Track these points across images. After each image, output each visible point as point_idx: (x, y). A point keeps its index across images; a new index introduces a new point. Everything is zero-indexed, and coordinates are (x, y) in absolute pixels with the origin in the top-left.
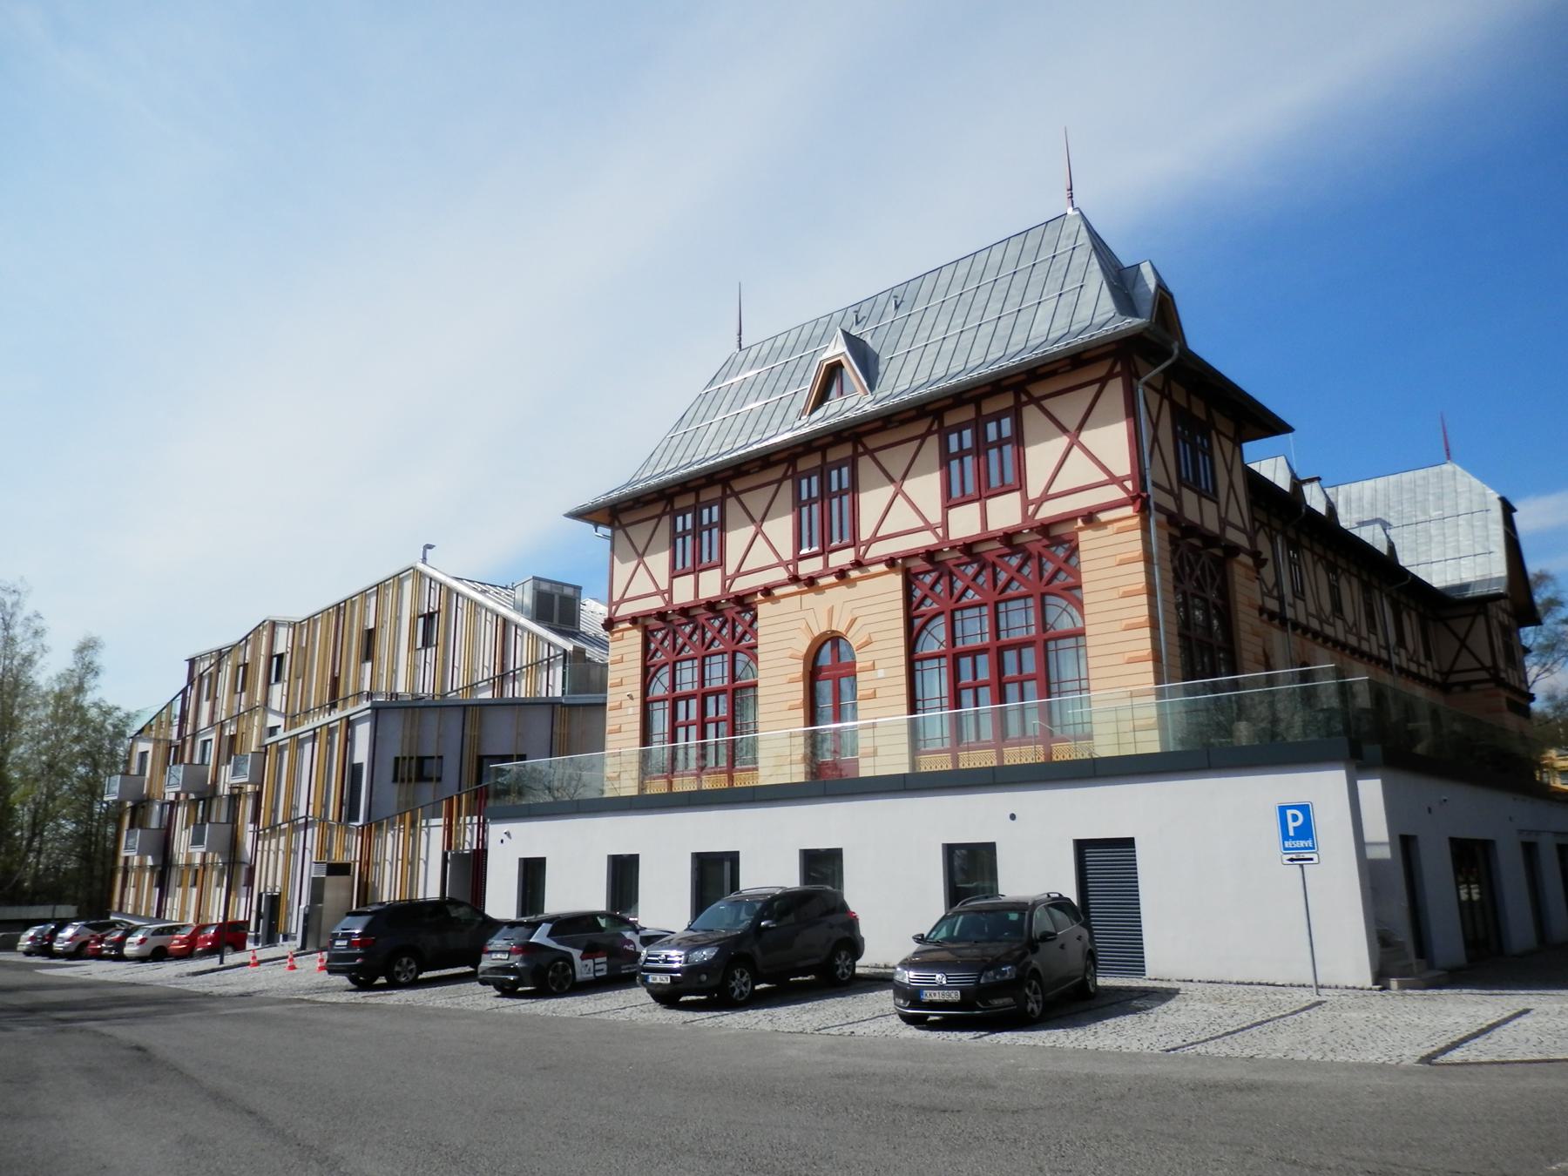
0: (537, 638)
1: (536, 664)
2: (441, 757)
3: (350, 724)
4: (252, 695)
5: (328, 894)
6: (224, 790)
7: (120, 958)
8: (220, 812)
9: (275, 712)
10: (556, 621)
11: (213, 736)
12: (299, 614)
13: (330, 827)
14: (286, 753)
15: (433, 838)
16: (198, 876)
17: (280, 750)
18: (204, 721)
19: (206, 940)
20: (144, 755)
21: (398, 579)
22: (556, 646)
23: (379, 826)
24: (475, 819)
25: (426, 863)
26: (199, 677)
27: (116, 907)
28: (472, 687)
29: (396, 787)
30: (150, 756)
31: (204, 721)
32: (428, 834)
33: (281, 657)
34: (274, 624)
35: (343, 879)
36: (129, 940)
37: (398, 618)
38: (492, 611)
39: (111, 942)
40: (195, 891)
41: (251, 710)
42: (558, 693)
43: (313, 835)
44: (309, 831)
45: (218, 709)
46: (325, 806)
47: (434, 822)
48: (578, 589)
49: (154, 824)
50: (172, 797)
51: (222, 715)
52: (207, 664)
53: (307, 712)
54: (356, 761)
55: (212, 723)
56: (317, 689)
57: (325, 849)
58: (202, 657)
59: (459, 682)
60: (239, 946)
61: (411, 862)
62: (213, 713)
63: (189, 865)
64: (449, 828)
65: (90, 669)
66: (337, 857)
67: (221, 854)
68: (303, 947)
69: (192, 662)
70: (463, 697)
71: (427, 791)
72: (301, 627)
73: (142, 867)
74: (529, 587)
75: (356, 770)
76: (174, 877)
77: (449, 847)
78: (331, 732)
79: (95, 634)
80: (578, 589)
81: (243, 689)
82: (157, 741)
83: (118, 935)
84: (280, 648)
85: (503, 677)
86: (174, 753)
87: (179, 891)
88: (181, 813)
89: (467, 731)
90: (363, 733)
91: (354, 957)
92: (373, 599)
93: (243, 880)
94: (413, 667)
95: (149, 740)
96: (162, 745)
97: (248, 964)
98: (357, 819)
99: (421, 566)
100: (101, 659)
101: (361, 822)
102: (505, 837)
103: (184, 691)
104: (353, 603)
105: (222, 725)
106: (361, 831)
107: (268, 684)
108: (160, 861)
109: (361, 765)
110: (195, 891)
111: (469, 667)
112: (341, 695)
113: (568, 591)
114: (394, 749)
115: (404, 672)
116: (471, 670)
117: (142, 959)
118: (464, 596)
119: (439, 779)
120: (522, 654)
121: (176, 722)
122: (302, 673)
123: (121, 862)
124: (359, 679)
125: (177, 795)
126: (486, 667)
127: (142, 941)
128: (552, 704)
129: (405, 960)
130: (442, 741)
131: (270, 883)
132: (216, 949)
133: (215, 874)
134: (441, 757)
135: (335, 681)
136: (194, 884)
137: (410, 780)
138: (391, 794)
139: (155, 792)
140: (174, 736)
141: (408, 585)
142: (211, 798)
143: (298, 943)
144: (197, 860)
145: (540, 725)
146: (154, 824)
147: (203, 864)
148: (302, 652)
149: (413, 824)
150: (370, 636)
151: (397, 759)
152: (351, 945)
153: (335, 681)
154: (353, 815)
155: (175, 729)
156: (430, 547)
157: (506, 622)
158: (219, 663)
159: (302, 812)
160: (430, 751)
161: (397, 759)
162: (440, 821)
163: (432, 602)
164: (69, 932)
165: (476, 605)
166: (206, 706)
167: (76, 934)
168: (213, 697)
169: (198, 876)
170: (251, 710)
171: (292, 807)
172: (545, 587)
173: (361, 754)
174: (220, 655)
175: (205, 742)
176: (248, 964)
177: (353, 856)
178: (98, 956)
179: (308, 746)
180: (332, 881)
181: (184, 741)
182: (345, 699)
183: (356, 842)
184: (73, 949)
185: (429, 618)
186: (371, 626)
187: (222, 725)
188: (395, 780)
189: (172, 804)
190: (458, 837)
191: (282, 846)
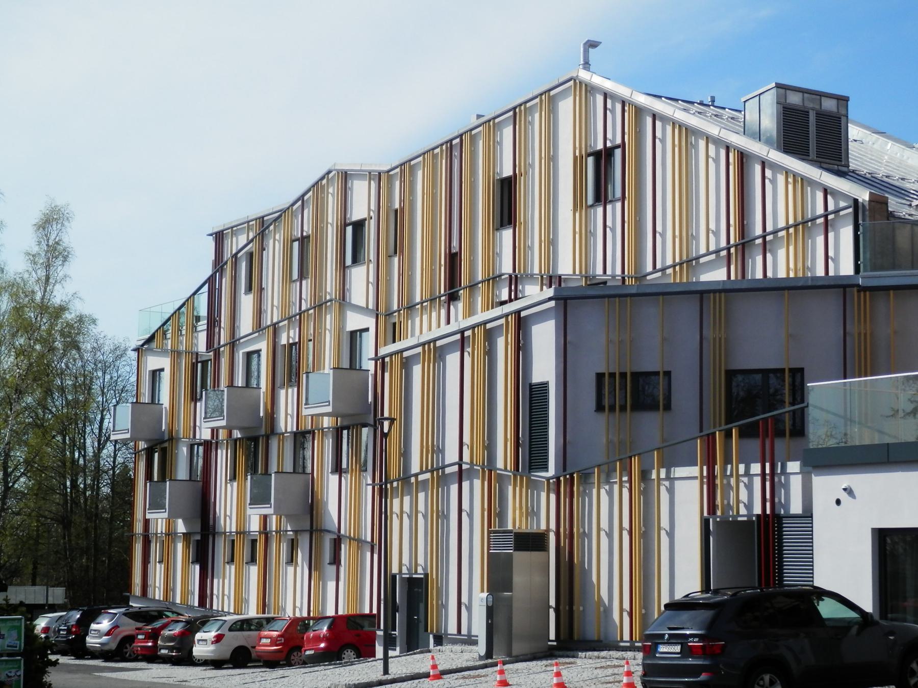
0: (804, 182)
1: (803, 225)
2: (668, 374)
3: (521, 325)
4: (318, 286)
5: (518, 579)
6: (286, 423)
7: (185, 658)
8: (280, 456)
9: (357, 309)
10: (813, 154)
11: (263, 346)
12: (384, 159)
13: (500, 478)
14: (417, 370)
15: (684, 499)
16: (255, 549)
17: (407, 364)
18: (246, 325)
19: (318, 639)
20: (155, 374)
21: (549, 99)
22: (836, 194)
23: (585, 477)
24: (756, 468)
25: (671, 535)
26: (233, 262)
27: (137, 590)
28: (690, 263)
29: (602, 418)
30: (166, 377)
31: (246, 325)
32: (671, 491)
33: (359, 226)
34: (345, 176)
35: (535, 556)
36: (198, 636)
37: (552, 159)
38: (718, 142)
39: (171, 638)
40: (254, 571)
41: (319, 306)
42: (846, 268)
43: (476, 489)
44: (466, 485)
45: (267, 306)
46: (490, 447)
47: (679, 472)
48: (843, 100)
49: (182, 473)
50: (206, 435)
51: (272, 315)
52: (242, 240)
53: (411, 308)
54: (536, 378)
55: (259, 327)
56: (423, 269)
57: (495, 511)
58: (234, 230)
59: (669, 255)
60: (365, 651)
61: (644, 536)
62: (259, 312)
63: (241, 533)
64: (711, 482)
65: (54, 254)
66: (514, 521)
67: (289, 517)
68: (489, 654)
69: (219, 237)
70: (672, 278)
71: (650, 425)
72: (390, 179)
73: (171, 534)
74: (769, 104)
75: (538, 393)
76: (221, 549)
77: (712, 508)
78: (490, 336)
79: (60, 202)
80: (843, 100)
81: (302, 276)
82: (176, 354)
83: (177, 629)
84: (358, 212)
85: (744, 245)
86: (199, 376)
87: (231, 570)
88: (222, 458)
89: (852, 328)
90: (544, 338)
91: (693, 671)
92: (508, 132)
93: (327, 556)
94: (585, 237)
95: (163, 352)
96: (184, 362)
97: (427, 675)
98: (545, 468)
99: (584, 75)
100: (71, 237)
101: (551, 472)
102: (844, 497)
103: (211, 281)
104: (473, 139)
105: (275, 329)
106: (555, 486)
107: (343, 268)
108: (198, 528)
109: (544, 386)
110: (254, 571)
111: (682, 227)
112: (464, 281)
113: (829, 105)
114: (595, 360)
115: (567, 240)
116: (688, 237)
117: (216, 664)
118: (665, 119)
119: (668, 407)
120: (776, 206)
121: (203, 325)
122: (398, 244)
123: (139, 528)
124: (493, 255)
125: (214, 431)
126: (712, 228)
127: (219, 638)
128: (841, 286)
129: (767, 678)
130: (666, 346)
131: (406, 560)
132: (331, 655)
133: (284, 547)
134: (668, 374)
135: (453, 260)
136: (253, 560)
137: (623, 408)
138: (597, 430)
139: (181, 428)
140: (202, 347)
141: (566, 108)
142: (267, 437)
143: (482, 648)
144: (255, 526)
145: (824, 319)
146: (182, 473)
147: (265, 531)
148: (399, 220)
149: (645, 475)
150: (506, 194)
151: (600, 377)
152: (687, 651)
153: (453, 260)
154: (537, 460)
155: (202, 338)
156: (592, 44)
157: (743, 158)
158: (262, 235)
159: (451, 456)
160: (650, 363)
161: (600, 377)
162: (694, 471)
163: (609, 131)
164: (104, 624)
165: (688, 132)
166: (247, 303)
167: (115, 627)
168: (254, 285)
169: (255, 549)
170: (319, 306)
171: (436, 449)
172: (794, 99)
173: (544, 367)
174: (262, 227)
175: (249, 355)
176: (427, 675)
177: (546, 519)
178: (152, 657)
179: (453, 360)
180: (522, 559)
181: (217, 354)
182: (472, 287)
183: (547, 503)
184: (113, 646)
185: (603, 158)
186: (507, 172)
187: (275, 329)
188: (600, 408)
189: (207, 445)
190: (725, 496)
191: (406, 508)
